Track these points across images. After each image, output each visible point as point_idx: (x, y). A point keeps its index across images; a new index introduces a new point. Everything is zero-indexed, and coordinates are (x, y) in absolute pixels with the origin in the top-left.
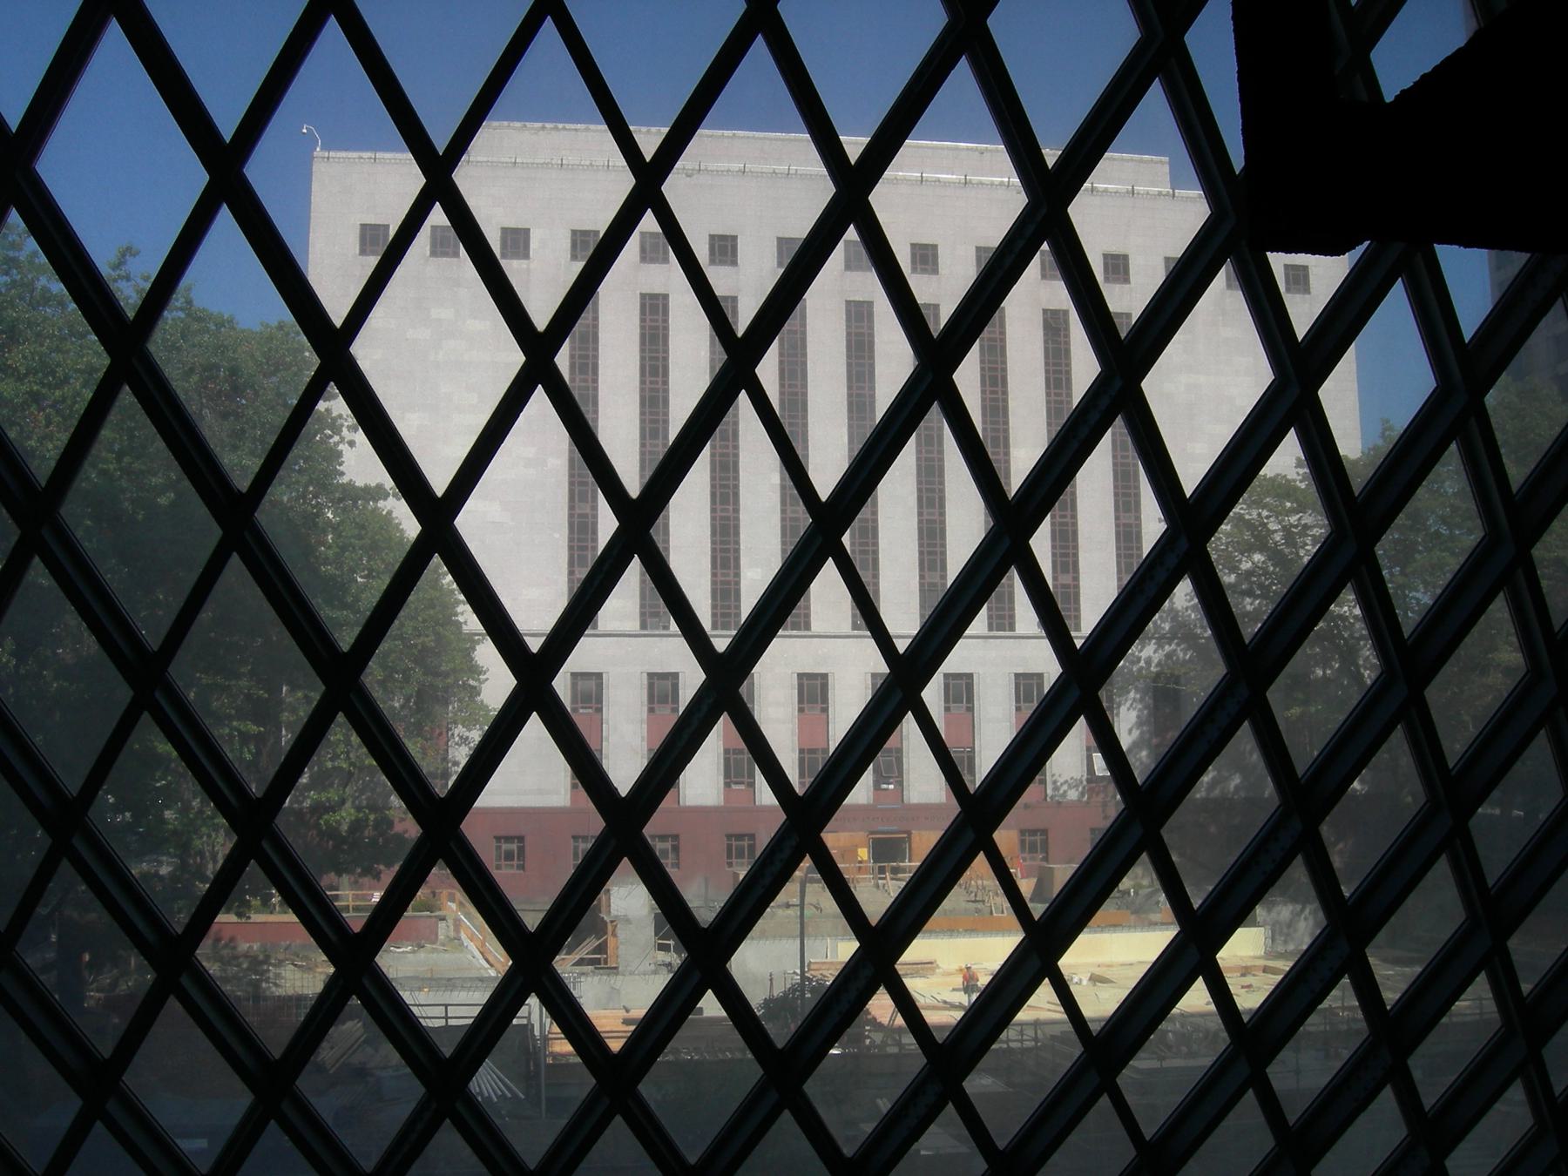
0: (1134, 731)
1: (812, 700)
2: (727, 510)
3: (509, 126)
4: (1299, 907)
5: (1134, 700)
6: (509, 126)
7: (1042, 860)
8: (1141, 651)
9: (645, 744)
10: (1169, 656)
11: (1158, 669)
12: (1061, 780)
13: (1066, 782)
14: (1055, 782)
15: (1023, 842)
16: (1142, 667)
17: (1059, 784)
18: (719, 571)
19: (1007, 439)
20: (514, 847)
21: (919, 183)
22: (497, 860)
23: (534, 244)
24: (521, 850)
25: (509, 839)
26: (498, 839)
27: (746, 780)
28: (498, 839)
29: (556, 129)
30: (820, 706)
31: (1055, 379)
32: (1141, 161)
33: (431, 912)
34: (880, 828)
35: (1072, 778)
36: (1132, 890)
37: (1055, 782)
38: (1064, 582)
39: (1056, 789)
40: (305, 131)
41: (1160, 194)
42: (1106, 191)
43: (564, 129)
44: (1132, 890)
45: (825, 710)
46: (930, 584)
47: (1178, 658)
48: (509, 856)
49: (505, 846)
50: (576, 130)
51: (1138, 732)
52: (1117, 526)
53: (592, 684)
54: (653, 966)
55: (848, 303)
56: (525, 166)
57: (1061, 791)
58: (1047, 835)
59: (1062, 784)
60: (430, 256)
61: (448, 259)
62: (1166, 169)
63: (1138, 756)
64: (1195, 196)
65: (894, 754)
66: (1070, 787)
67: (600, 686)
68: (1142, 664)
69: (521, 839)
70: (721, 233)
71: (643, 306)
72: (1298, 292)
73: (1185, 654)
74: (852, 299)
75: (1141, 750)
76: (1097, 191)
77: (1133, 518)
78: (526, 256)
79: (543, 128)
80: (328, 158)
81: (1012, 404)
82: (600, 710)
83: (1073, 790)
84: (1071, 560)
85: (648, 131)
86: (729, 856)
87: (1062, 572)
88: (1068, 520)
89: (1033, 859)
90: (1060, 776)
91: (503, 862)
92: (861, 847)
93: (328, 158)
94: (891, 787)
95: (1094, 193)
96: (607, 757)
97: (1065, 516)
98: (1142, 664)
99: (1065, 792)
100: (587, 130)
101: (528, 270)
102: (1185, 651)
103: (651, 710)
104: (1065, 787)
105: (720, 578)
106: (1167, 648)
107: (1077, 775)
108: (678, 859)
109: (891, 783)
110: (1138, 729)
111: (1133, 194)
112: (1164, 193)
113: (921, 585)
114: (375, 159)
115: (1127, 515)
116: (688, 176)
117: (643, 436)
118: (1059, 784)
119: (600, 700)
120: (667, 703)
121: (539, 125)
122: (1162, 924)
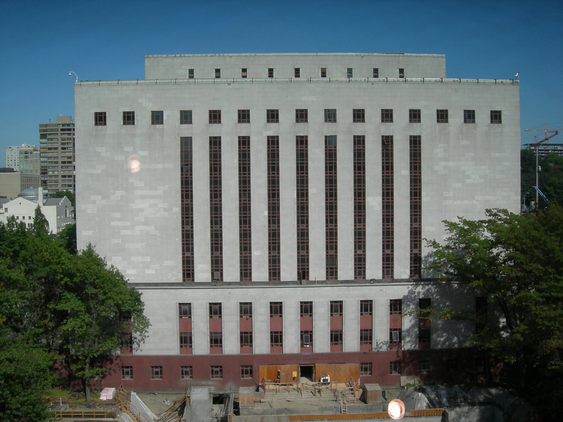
0: (412, 320)
1: (276, 312)
2: (246, 227)
3: (161, 56)
4: (470, 407)
5: (412, 308)
6: (161, 56)
7: (370, 374)
8: (416, 289)
9: (209, 331)
10: (428, 290)
11: (423, 296)
12: (380, 342)
13: (382, 342)
14: (377, 343)
15: (362, 368)
16: (416, 296)
17: (379, 343)
18: (243, 252)
19: (364, 193)
20: (159, 370)
21: (329, 82)
22: (152, 375)
23: (165, 118)
24: (161, 371)
25: (156, 367)
26: (152, 367)
27: (249, 344)
28: (152, 367)
29: (181, 56)
30: (279, 314)
31: (331, 272)
32: (434, 57)
33: (114, 418)
34: (304, 363)
35: (384, 341)
36: (406, 387)
37: (377, 343)
38: (387, 253)
39: (377, 345)
40: (70, 74)
41: (436, 81)
42: (411, 81)
43: (184, 56)
44: (406, 387)
45: (281, 316)
46: (331, 255)
47: (432, 291)
48: (157, 373)
49: (155, 370)
50: (189, 56)
51: (414, 321)
52: (411, 228)
53: (187, 307)
54: (211, 418)
55: (297, 137)
56: (161, 84)
57: (380, 346)
58: (372, 365)
59: (380, 344)
60: (123, 125)
61: (130, 126)
62: (444, 60)
63: (413, 331)
64: (452, 81)
65: (309, 333)
66: (383, 344)
67: (190, 308)
68: (416, 294)
69: (161, 367)
70: (243, 109)
71: (210, 142)
72: (496, 122)
73: (435, 290)
74: (299, 135)
75: (415, 328)
76: (408, 81)
77: (418, 225)
78: (162, 123)
79: (175, 57)
80: (81, 85)
81: (367, 179)
82: (190, 317)
83: (385, 346)
84: (390, 243)
85: (219, 55)
86: (242, 373)
87: (386, 249)
88: (390, 226)
89: (366, 374)
90: (379, 340)
91: (155, 376)
92: (294, 371)
93: (81, 85)
94: (308, 346)
95: (407, 82)
96: (194, 336)
97: (388, 225)
98: (416, 294)
99: (381, 346)
100: (193, 56)
101: (163, 129)
102: (435, 288)
103: (211, 317)
104: (381, 344)
105: (243, 255)
106: (427, 287)
107: (386, 340)
108: (222, 374)
109: (308, 345)
110: (414, 320)
111: (424, 82)
112: (438, 81)
113: (327, 256)
114: (99, 84)
115: (415, 223)
116: (229, 84)
117: (211, 197)
118: (379, 343)
119: (190, 313)
120: (217, 314)
121: (173, 55)
122: (410, 417)
